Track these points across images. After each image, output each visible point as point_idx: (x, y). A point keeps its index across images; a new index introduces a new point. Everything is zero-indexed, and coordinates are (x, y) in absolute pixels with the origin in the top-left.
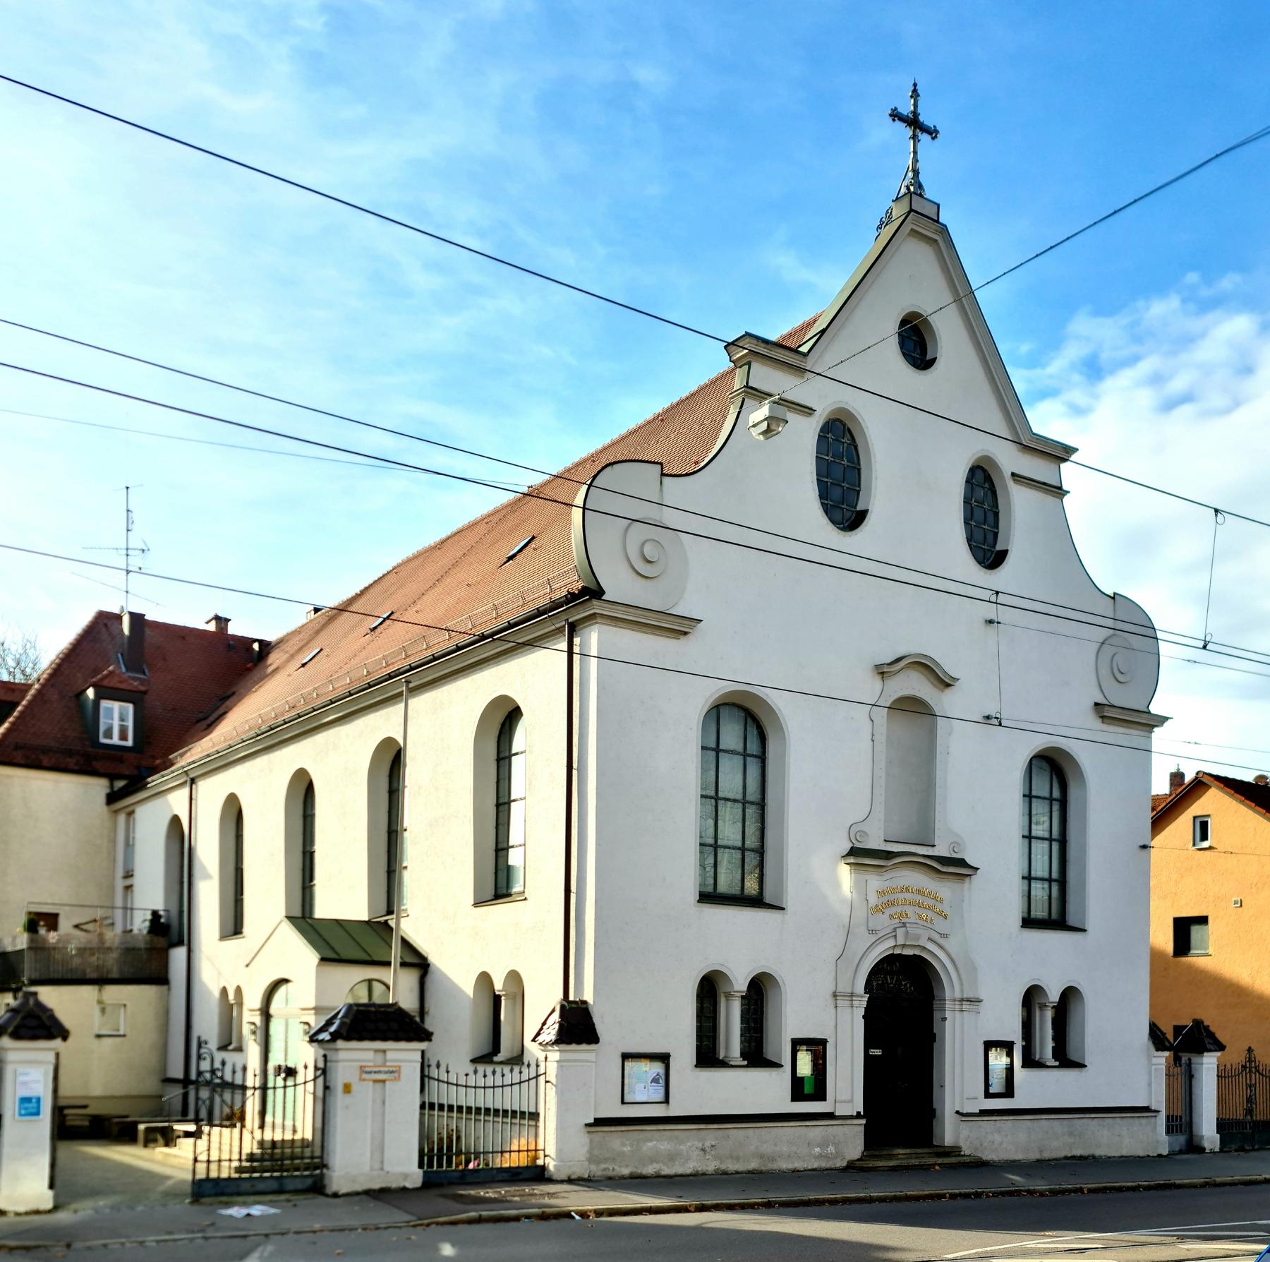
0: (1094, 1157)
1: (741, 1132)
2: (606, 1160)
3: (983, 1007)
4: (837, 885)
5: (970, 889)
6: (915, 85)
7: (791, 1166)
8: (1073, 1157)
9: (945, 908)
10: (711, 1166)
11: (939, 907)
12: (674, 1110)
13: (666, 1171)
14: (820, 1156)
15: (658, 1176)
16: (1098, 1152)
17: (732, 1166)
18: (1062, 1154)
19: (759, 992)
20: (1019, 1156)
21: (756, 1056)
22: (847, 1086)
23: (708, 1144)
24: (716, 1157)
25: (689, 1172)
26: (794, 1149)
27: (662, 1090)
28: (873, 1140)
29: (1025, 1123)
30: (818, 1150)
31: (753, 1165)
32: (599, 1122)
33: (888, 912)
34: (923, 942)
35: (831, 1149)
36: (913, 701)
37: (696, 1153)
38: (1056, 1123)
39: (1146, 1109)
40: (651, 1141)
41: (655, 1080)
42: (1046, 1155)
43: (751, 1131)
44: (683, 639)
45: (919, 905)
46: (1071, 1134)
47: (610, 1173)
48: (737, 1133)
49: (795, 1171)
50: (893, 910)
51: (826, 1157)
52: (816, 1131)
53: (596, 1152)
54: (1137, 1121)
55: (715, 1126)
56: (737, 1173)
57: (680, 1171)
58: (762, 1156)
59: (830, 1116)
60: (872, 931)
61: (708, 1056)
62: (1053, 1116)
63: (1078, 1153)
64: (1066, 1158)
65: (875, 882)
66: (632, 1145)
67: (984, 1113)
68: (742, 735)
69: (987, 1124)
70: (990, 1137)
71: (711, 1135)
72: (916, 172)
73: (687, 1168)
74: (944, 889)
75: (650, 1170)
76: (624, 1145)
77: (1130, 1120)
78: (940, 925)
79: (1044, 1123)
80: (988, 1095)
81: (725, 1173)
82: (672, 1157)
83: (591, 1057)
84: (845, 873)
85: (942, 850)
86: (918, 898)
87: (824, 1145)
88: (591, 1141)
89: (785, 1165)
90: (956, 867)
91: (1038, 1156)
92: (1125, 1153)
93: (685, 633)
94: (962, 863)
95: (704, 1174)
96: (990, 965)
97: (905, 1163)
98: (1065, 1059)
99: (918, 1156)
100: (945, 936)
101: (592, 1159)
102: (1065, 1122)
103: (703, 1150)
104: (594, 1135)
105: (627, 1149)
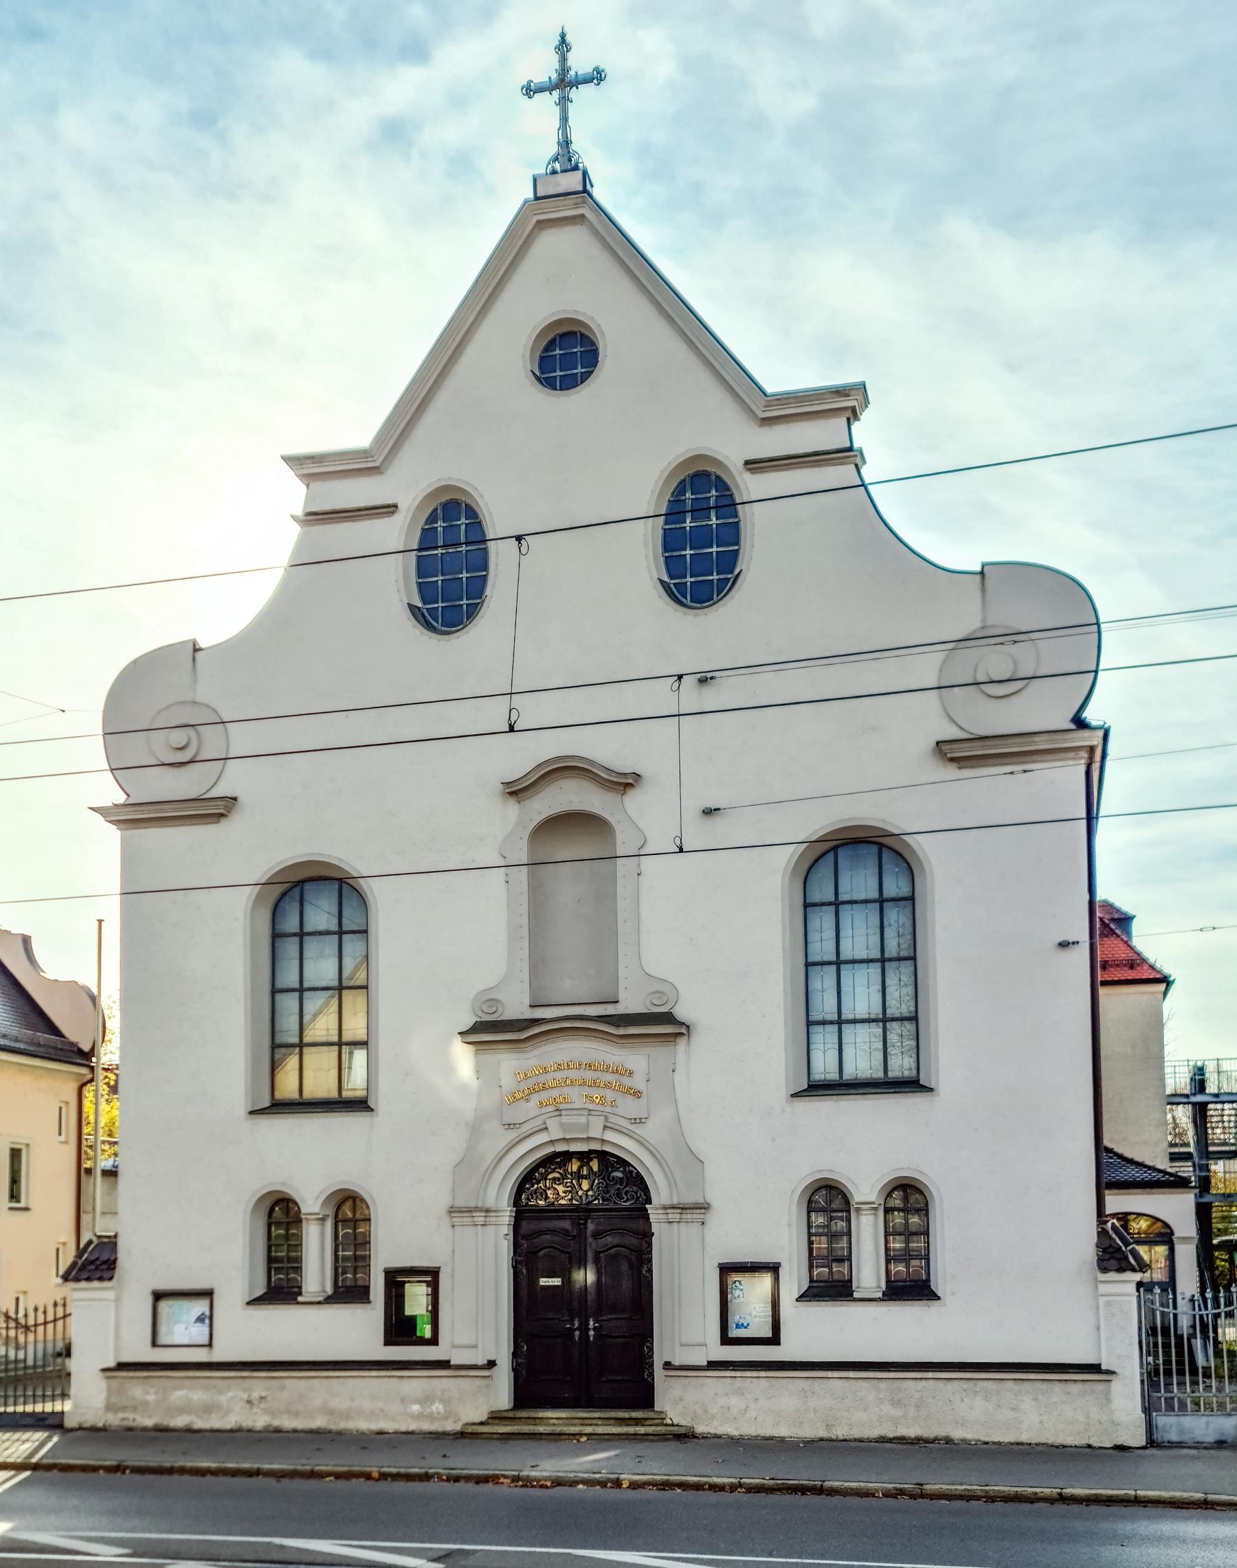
0: (948, 1440)
1: (303, 1383)
2: (125, 1409)
3: (713, 1219)
4: (448, 1068)
5: (688, 1053)
6: (563, 36)
7: (375, 1426)
8: (902, 1440)
9: (638, 1082)
10: (259, 1421)
11: (627, 1081)
12: (218, 1355)
13: (199, 1424)
14: (420, 1416)
15: (189, 1431)
16: (957, 1434)
17: (288, 1423)
18: (874, 1433)
19: (349, 1211)
20: (783, 1431)
21: (349, 1291)
22: (478, 1317)
23: (255, 1396)
24: (266, 1412)
25: (228, 1427)
26: (380, 1404)
27: (206, 1330)
28: (529, 1393)
29: (796, 1383)
30: (416, 1408)
31: (319, 1422)
32: (122, 1366)
33: (535, 1099)
34: (596, 1132)
35: (438, 1407)
36: (571, 821)
37: (240, 1406)
38: (864, 1384)
39: (1095, 1368)
40: (181, 1389)
41: (200, 1319)
42: (840, 1432)
43: (316, 1382)
44: (224, 823)
45: (594, 1084)
46: (896, 1403)
47: (130, 1424)
48: (295, 1384)
49: (381, 1433)
50: (544, 1095)
51: (431, 1417)
52: (414, 1385)
53: (113, 1399)
54: (1058, 1386)
55: (263, 1374)
56: (295, 1431)
57: (217, 1424)
58: (331, 1412)
59: (444, 1365)
60: (510, 1126)
61: (280, 1289)
62: (851, 1374)
63: (912, 1432)
64: (882, 1440)
65: (509, 1065)
66: (156, 1393)
67: (713, 1365)
68: (818, 908)
69: (716, 1384)
70: (722, 1401)
71: (259, 1385)
72: (565, 143)
73: (229, 1422)
74: (637, 1060)
75: (179, 1422)
76: (147, 1393)
77: (1044, 1386)
78: (628, 1107)
79: (836, 1383)
80: (726, 1340)
81: (278, 1430)
82: (208, 1409)
83: (111, 1295)
84: (463, 1057)
85: (630, 1003)
86: (589, 1075)
87: (427, 1399)
88: (109, 1388)
89: (364, 1425)
90: (662, 1025)
91: (822, 1433)
92: (1024, 1438)
93: (222, 815)
94: (668, 1018)
95: (250, 1430)
96: (733, 1150)
97: (558, 1429)
98: (910, 1286)
99: (584, 1422)
100: (638, 1121)
101: (110, 1408)
102: (883, 1385)
103: (249, 1402)
104: (112, 1381)
105: (151, 1397)
